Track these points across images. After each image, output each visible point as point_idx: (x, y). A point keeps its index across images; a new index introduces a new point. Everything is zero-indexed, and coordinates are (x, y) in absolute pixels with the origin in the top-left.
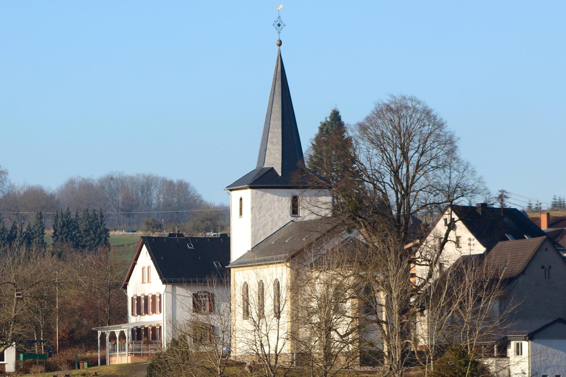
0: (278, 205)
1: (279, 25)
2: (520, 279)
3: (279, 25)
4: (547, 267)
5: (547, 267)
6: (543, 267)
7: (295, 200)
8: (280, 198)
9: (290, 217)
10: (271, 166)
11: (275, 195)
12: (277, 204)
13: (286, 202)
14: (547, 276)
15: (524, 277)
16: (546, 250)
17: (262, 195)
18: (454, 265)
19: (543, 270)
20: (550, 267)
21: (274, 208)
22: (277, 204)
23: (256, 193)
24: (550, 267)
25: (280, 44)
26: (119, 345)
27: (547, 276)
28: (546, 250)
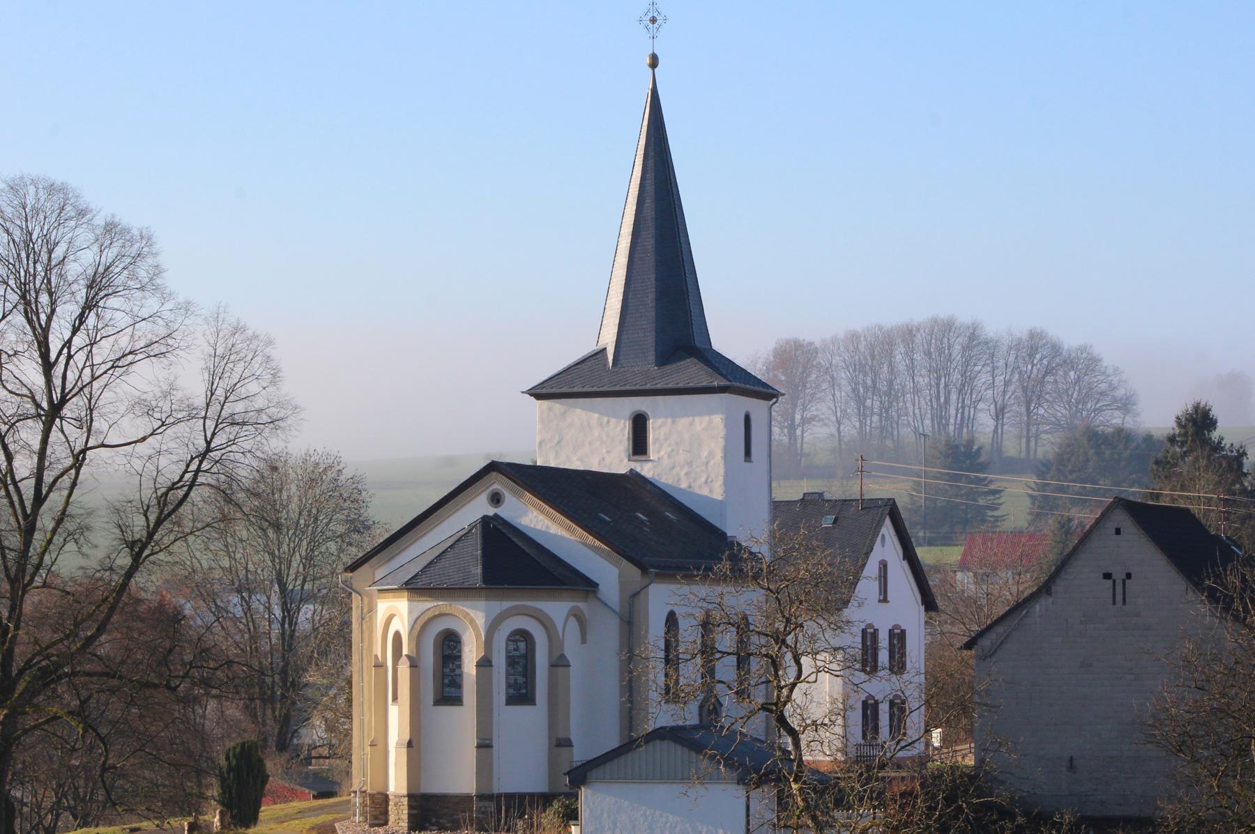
1: (653, 20)
2: (1038, 607)
3: (653, 20)
4: (1119, 576)
5: (1119, 576)
6: (1107, 576)
7: (639, 425)
8: (605, 419)
9: (626, 461)
11: (594, 411)
14: (1119, 598)
15: (1050, 600)
16: (1118, 531)
19: (1110, 582)
20: (1129, 576)
21: (590, 443)
23: (550, 409)
24: (1129, 576)
25: (654, 62)
27: (1119, 598)
28: (1118, 531)
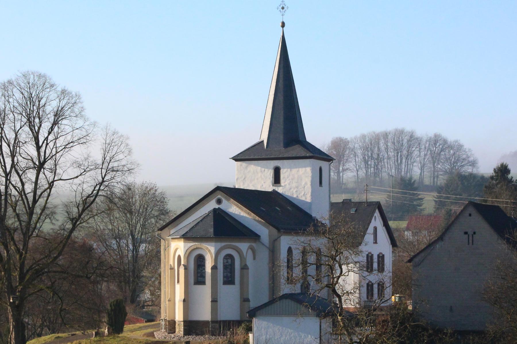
0: (261, 176)
2: (438, 246)
4: (470, 233)
5: (470, 233)
6: (466, 233)
7: (277, 172)
8: (263, 169)
10: (287, 149)
11: (258, 166)
12: (260, 175)
13: (270, 174)
14: (471, 241)
16: (470, 215)
17: (246, 167)
18: (297, 234)
19: (466, 236)
20: (474, 233)
21: (257, 179)
22: (260, 175)
23: (241, 165)
25: (283, 25)
26: (13, 315)
27: (471, 241)
28: (470, 215)
